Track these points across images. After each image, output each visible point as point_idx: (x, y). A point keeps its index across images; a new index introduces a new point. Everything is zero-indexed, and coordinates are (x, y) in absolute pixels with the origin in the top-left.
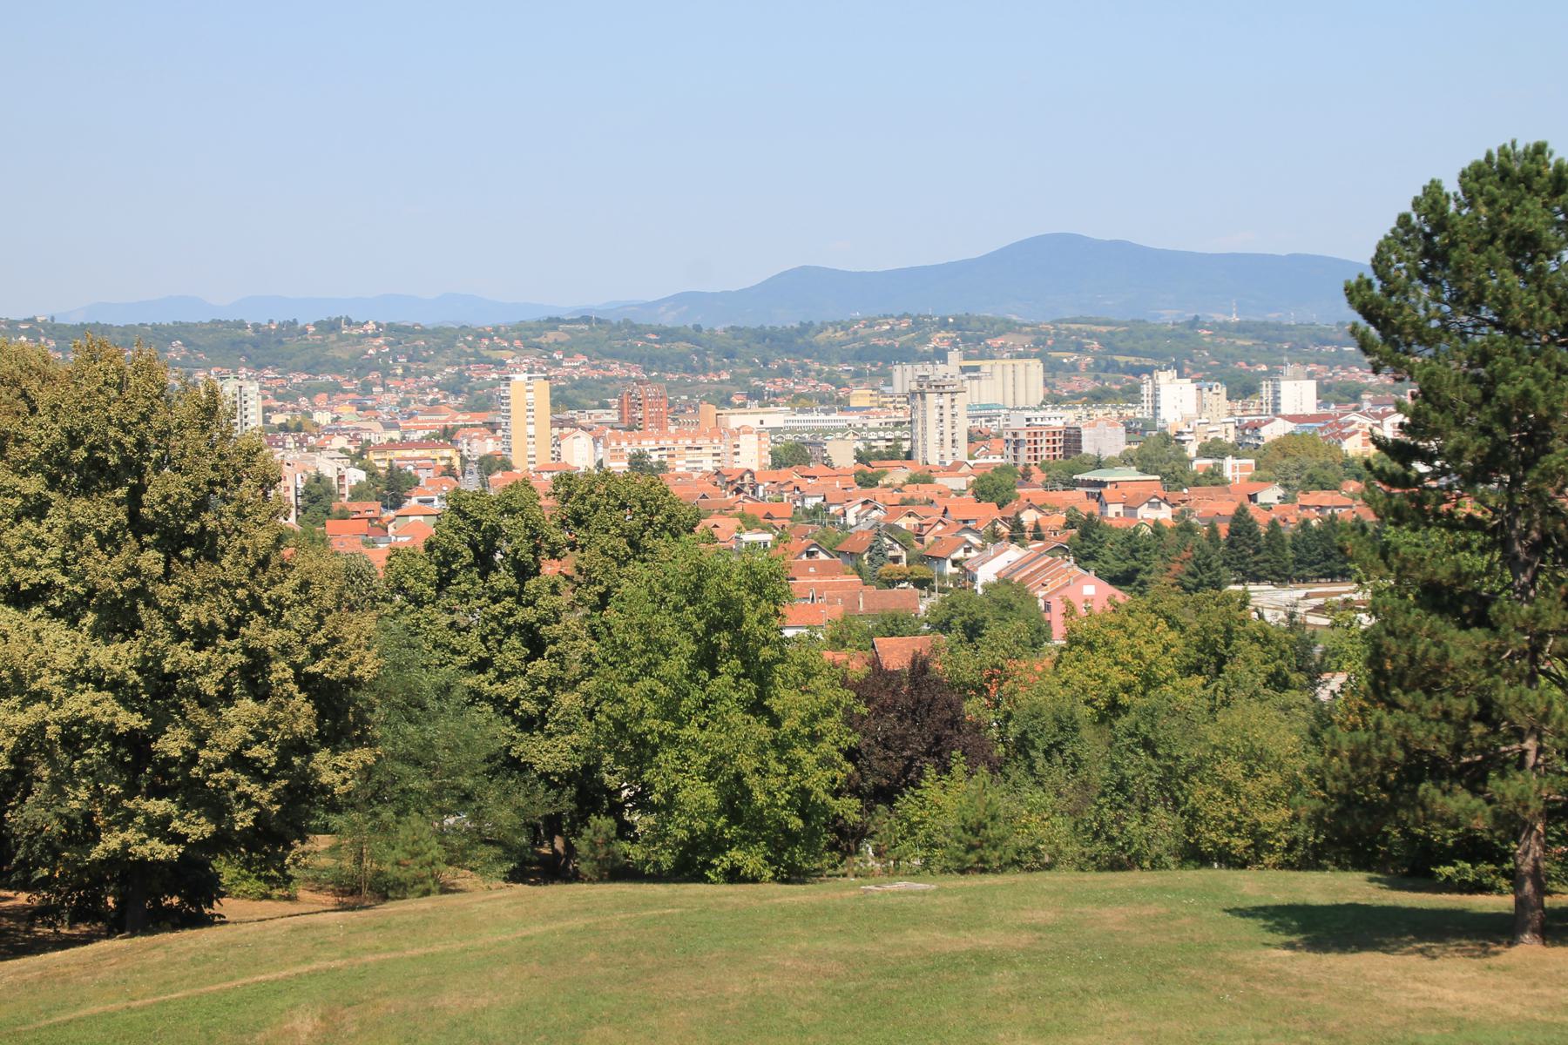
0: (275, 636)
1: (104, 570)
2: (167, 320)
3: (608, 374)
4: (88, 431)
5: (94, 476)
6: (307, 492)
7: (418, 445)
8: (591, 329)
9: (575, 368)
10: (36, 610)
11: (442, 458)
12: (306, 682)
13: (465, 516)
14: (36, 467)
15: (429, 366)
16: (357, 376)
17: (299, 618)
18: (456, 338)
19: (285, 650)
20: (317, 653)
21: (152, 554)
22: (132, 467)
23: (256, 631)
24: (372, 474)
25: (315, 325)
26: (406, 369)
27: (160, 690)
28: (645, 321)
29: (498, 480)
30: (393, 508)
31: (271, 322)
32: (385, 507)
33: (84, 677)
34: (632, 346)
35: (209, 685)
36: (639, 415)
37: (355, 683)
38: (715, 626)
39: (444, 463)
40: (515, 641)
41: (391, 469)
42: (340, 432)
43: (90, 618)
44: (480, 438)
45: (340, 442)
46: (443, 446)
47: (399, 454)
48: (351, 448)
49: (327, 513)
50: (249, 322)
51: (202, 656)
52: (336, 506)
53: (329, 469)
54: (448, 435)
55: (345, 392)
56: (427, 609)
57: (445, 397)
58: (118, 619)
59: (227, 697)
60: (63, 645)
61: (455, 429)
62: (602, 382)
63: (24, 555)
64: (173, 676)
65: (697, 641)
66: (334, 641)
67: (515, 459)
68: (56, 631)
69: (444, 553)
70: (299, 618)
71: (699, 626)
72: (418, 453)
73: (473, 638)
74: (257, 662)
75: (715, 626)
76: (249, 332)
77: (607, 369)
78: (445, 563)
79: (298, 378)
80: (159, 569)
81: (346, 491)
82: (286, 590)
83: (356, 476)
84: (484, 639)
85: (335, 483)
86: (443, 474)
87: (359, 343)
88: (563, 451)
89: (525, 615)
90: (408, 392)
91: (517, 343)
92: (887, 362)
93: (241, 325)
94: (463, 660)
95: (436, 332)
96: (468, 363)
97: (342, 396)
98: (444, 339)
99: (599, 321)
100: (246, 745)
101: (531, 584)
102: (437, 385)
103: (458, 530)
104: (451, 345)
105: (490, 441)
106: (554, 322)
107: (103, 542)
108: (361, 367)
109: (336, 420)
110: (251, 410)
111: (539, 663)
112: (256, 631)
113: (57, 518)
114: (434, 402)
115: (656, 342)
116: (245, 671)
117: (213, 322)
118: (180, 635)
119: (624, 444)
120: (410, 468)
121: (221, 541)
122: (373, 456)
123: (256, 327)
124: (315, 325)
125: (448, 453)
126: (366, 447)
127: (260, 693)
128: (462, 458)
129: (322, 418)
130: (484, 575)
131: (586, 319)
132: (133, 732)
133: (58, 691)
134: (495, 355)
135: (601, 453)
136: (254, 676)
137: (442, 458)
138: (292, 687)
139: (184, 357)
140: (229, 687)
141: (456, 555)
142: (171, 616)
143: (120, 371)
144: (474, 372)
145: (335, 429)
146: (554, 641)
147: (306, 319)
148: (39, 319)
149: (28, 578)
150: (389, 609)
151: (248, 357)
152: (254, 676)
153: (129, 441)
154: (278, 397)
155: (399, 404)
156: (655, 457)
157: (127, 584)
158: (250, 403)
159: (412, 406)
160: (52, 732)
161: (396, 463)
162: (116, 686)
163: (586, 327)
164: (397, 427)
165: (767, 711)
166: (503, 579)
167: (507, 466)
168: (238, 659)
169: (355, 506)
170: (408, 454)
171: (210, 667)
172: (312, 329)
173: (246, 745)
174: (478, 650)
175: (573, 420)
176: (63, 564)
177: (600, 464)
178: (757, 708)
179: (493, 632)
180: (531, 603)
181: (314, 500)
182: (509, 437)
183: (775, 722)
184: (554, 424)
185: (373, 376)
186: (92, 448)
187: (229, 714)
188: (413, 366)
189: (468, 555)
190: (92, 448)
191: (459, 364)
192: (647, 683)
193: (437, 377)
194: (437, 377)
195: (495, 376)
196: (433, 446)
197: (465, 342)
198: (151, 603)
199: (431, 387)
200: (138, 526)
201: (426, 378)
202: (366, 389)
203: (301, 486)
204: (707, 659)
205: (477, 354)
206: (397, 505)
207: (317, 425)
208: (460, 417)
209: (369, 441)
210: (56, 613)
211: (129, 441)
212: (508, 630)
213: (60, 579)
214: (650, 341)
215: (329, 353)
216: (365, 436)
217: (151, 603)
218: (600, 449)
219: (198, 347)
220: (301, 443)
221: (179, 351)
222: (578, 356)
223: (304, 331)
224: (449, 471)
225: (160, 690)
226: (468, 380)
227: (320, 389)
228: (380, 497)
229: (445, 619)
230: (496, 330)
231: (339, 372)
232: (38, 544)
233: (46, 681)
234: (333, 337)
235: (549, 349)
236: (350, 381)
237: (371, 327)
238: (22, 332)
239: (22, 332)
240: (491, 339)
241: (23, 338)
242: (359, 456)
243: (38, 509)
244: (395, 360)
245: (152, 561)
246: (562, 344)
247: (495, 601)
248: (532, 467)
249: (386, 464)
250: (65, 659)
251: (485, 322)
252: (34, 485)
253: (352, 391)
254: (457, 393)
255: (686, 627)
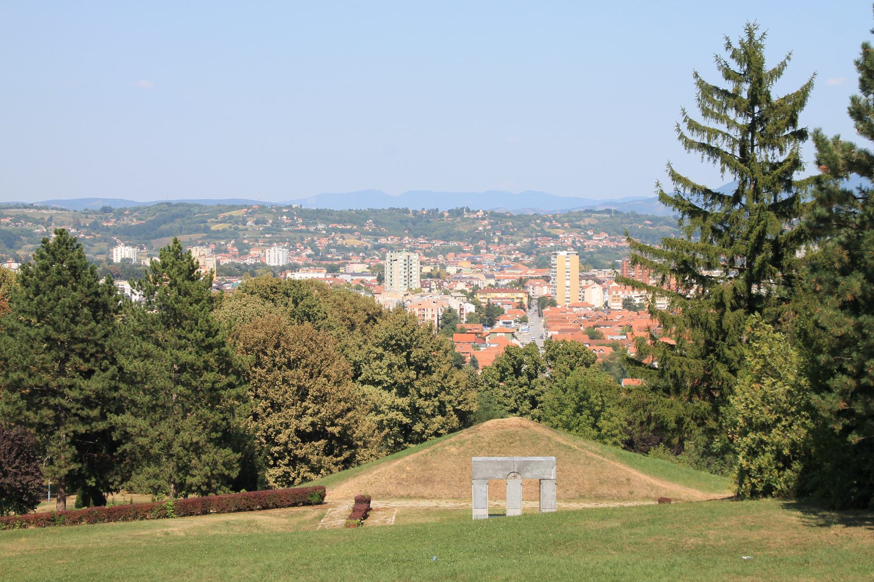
0: (448, 398)
1: (400, 376)
2: (364, 208)
3: (620, 244)
4: (396, 335)
5: (398, 348)
6: (444, 318)
7: (504, 289)
8: (611, 217)
9: (600, 240)
10: (380, 387)
11: (517, 298)
12: (456, 411)
13: (511, 355)
14: (381, 345)
15: (514, 238)
16: (471, 243)
17: (455, 392)
18: (530, 221)
19: (450, 402)
20: (460, 403)
21: (413, 372)
22: (408, 346)
23: (442, 396)
24: (478, 307)
25: (449, 212)
26: (500, 239)
27: (415, 412)
28: (644, 213)
29: (547, 312)
30: (489, 326)
31: (423, 209)
32: (484, 325)
33: (393, 407)
34: (636, 228)
35: (429, 411)
36: (633, 274)
37: (470, 412)
38: (581, 399)
39: (518, 301)
40: (527, 402)
41: (489, 305)
42: (461, 279)
43: (395, 390)
44: (540, 286)
45: (461, 286)
46: (519, 291)
47: (493, 295)
48: (467, 289)
49: (454, 329)
50: (411, 209)
51: (427, 403)
52: (458, 326)
53: (455, 304)
54: (521, 283)
55: (464, 252)
56: (496, 389)
57: (523, 257)
58: (403, 392)
59: (433, 416)
60: (389, 398)
61: (527, 279)
62: (616, 250)
63: (377, 371)
64: (418, 408)
65: (576, 404)
66: (465, 399)
67: (558, 299)
68: (385, 394)
69: (503, 368)
70: (455, 392)
71: (577, 399)
72: (504, 295)
73: (512, 400)
74: (442, 404)
75: (581, 399)
76: (411, 215)
77: (620, 242)
78: (502, 372)
79: (438, 243)
80: (415, 377)
81: (464, 317)
82: (452, 383)
83: (470, 308)
84: (516, 401)
85: (458, 313)
86: (517, 308)
87: (474, 223)
88: (586, 295)
89: (531, 392)
90: (501, 253)
91: (566, 225)
92: (748, 258)
93: (406, 211)
94: (508, 408)
95: (520, 217)
96: (537, 236)
97: (462, 254)
98: (523, 222)
99: (616, 212)
100: (439, 429)
101: (533, 381)
102: (518, 249)
103: (508, 360)
104: (527, 226)
105: (545, 288)
106: (589, 212)
107: (400, 367)
108: (475, 237)
109: (459, 271)
110: (414, 269)
111: (535, 410)
112: (442, 396)
113: (386, 362)
114: (516, 260)
115: (650, 225)
116: (439, 407)
117: (390, 209)
118: (420, 396)
119: (620, 293)
120: (499, 304)
121: (433, 369)
122: (478, 296)
123: (415, 212)
124: (449, 212)
125: (520, 295)
126: (476, 289)
127: (443, 414)
128: (529, 297)
129: (451, 270)
130: (517, 377)
131: (608, 211)
132: (407, 424)
133: (387, 411)
134: (553, 232)
135: (607, 297)
136: (441, 409)
137: (517, 298)
138: (452, 413)
139: (373, 229)
140: (434, 412)
141: (507, 369)
142: (418, 391)
143: (406, 318)
144: (540, 242)
145: (458, 278)
146: (541, 402)
147: (444, 208)
148: (294, 206)
149: (377, 378)
150: (482, 388)
151: (410, 230)
152: (441, 409)
153: (408, 339)
154: (426, 255)
155: (495, 261)
156: (638, 301)
157: (406, 381)
158: (414, 265)
159: (503, 262)
160: (385, 422)
161: (492, 301)
162: (403, 410)
163: (608, 216)
164: (492, 277)
165: (597, 426)
166: (524, 379)
167: (553, 304)
168: (437, 404)
169: (469, 326)
170: (499, 295)
171: (428, 406)
172: (446, 214)
173: (439, 429)
174: (513, 405)
175: (594, 275)
176: (387, 374)
177: (606, 304)
178: (594, 426)
179: (519, 398)
180: (533, 388)
181: (447, 322)
182: (555, 287)
183: (600, 430)
184: (581, 278)
185: (481, 243)
186: (397, 341)
187: (434, 420)
188: (504, 237)
189: (511, 369)
190: (397, 341)
191: (532, 237)
192: (559, 416)
193: (518, 245)
194: (518, 245)
195: (552, 244)
196: (512, 290)
197: (536, 224)
198: (412, 386)
199: (515, 250)
200: (409, 364)
201: (512, 245)
202: (477, 251)
203: (440, 314)
204: (579, 410)
205: (542, 231)
206: (491, 324)
207: (449, 274)
208: (530, 272)
209: (477, 286)
210: (384, 388)
211: (408, 339)
212: (525, 398)
213: (387, 379)
214: (645, 225)
215: (456, 229)
216: (475, 282)
217: (412, 386)
218: (607, 295)
219: (382, 224)
220: (439, 287)
221: (370, 226)
222: (602, 233)
223: (442, 215)
224: (521, 306)
225: (415, 412)
226: (536, 246)
227: (451, 250)
228: (482, 321)
229: (502, 393)
230: (554, 216)
231: (461, 240)
232: (380, 368)
233: (383, 408)
234: (459, 219)
235: (585, 229)
236: (468, 245)
237: (481, 214)
238: (284, 213)
239: (284, 213)
240: (551, 222)
241: (285, 217)
242: (472, 295)
243: (380, 357)
244: (494, 234)
245: (413, 374)
246: (593, 226)
247: (521, 387)
248: (567, 304)
249: (486, 301)
250: (389, 402)
251: (546, 209)
252: (380, 350)
253: (468, 252)
254: (530, 254)
255: (573, 399)
